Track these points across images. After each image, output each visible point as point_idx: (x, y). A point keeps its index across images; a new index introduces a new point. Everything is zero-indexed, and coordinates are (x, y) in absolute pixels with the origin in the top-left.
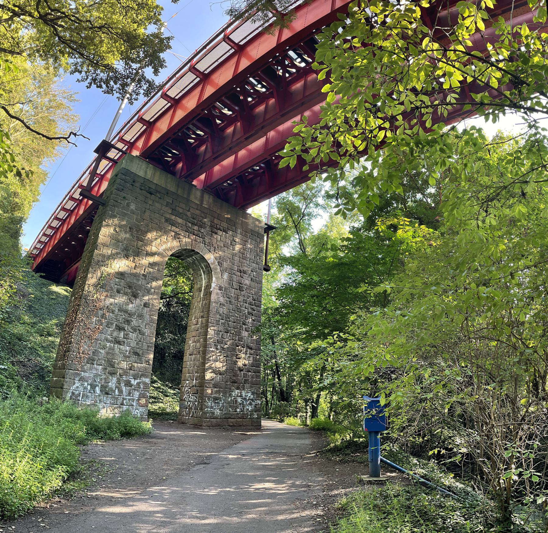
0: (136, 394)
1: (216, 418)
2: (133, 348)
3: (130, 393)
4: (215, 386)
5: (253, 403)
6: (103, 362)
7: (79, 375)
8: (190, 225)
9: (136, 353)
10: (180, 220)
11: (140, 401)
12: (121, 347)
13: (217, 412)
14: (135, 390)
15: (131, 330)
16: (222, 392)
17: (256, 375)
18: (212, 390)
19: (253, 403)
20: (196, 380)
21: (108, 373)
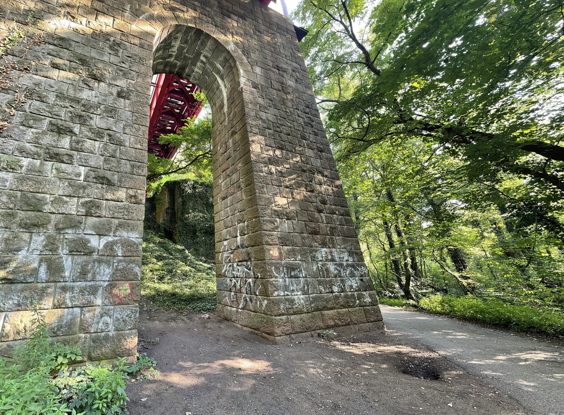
1: (298, 312)
2: (94, 169)
9: (103, 178)
11: (116, 291)
12: (63, 166)
14: (100, 262)
15: (89, 134)
16: (299, 252)
18: (279, 249)
20: (242, 234)
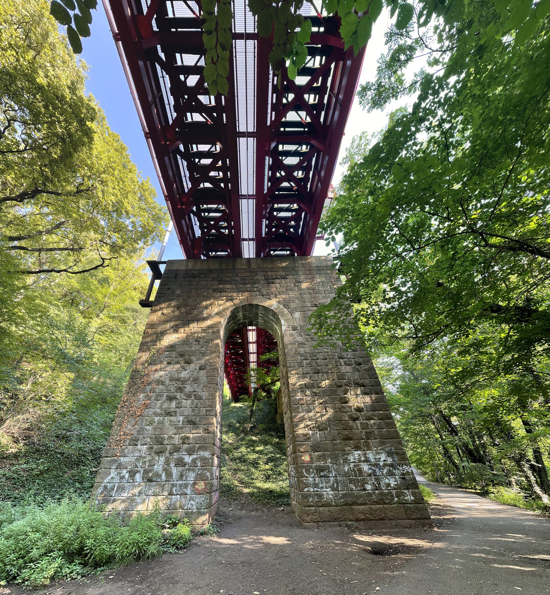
0: (192, 476)
1: (327, 505)
2: (187, 417)
3: (181, 476)
4: (315, 448)
5: (396, 472)
6: (149, 440)
7: (116, 461)
8: (242, 286)
9: (191, 421)
10: (228, 286)
12: (172, 418)
13: (328, 494)
14: (189, 470)
15: (184, 397)
16: (330, 456)
17: (386, 423)
19: (396, 472)
21: (155, 453)
